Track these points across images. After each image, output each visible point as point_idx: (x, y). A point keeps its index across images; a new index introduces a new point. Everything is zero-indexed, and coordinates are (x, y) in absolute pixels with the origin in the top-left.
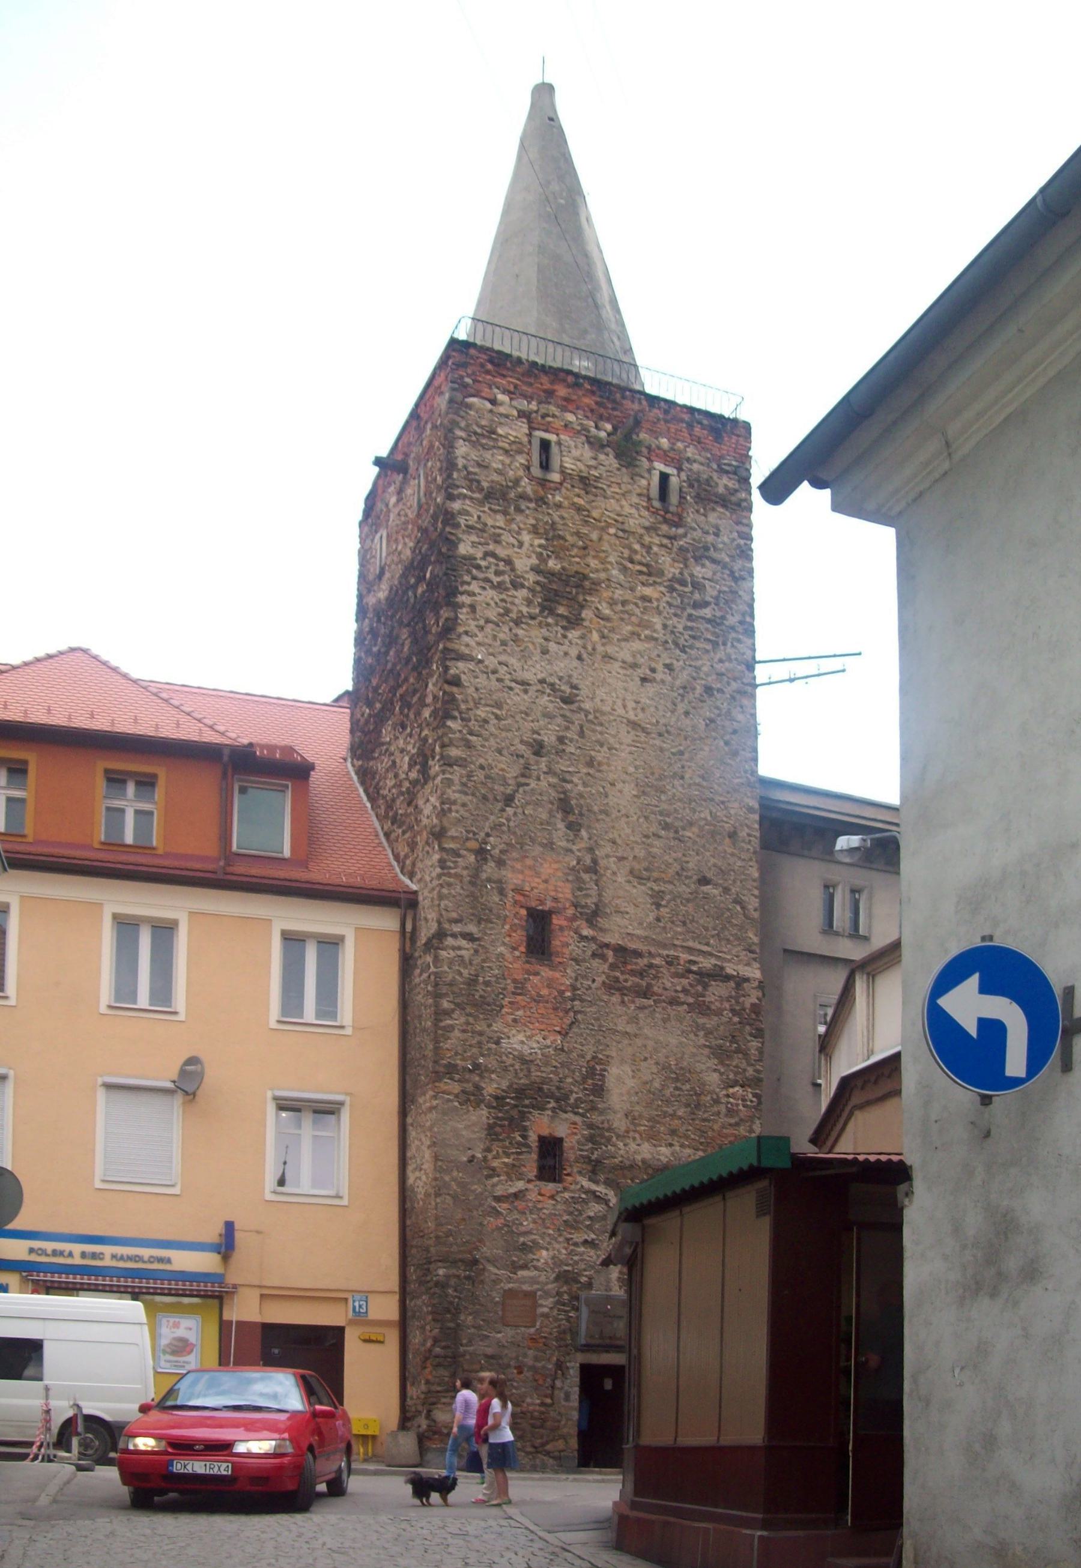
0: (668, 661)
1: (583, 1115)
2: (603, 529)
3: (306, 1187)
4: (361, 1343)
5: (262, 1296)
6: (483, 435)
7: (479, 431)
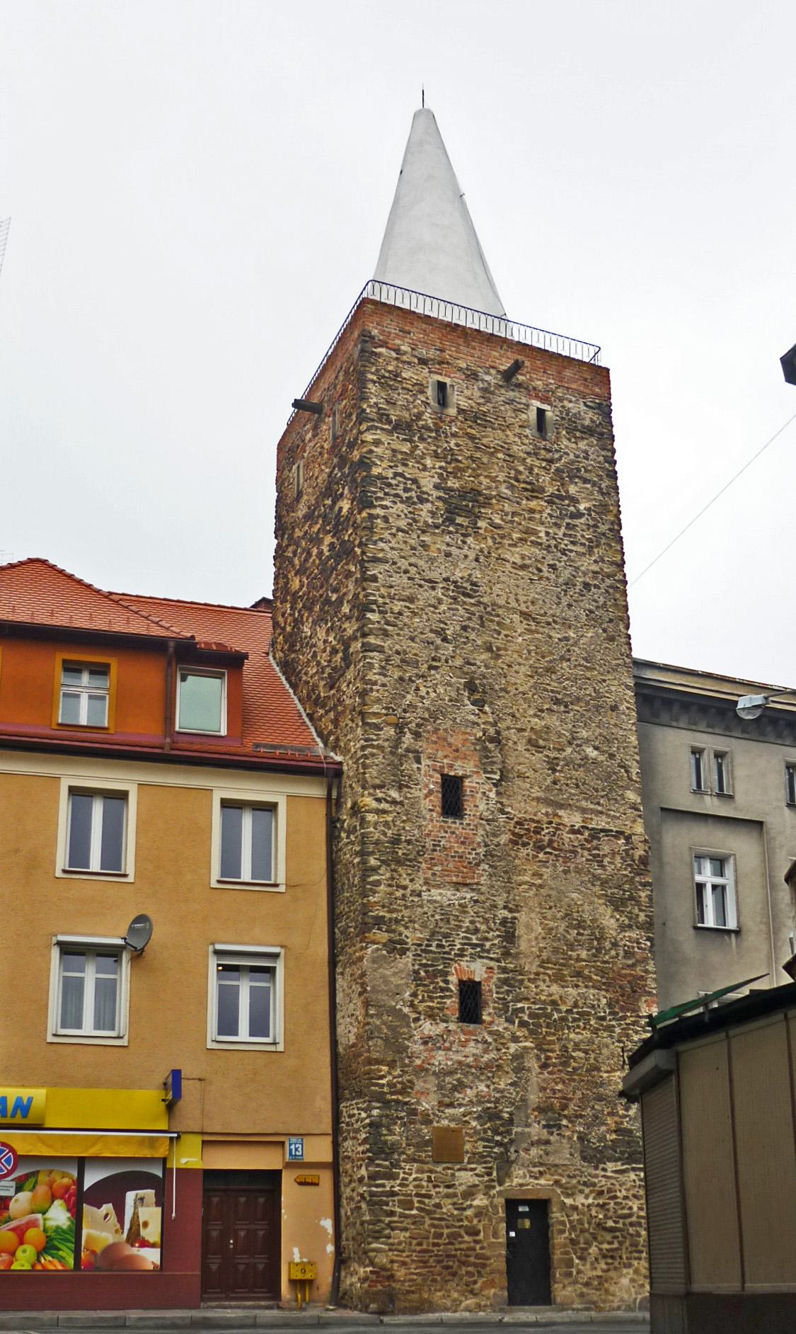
1: (498, 960)
2: (492, 454)
5: (204, 1142)
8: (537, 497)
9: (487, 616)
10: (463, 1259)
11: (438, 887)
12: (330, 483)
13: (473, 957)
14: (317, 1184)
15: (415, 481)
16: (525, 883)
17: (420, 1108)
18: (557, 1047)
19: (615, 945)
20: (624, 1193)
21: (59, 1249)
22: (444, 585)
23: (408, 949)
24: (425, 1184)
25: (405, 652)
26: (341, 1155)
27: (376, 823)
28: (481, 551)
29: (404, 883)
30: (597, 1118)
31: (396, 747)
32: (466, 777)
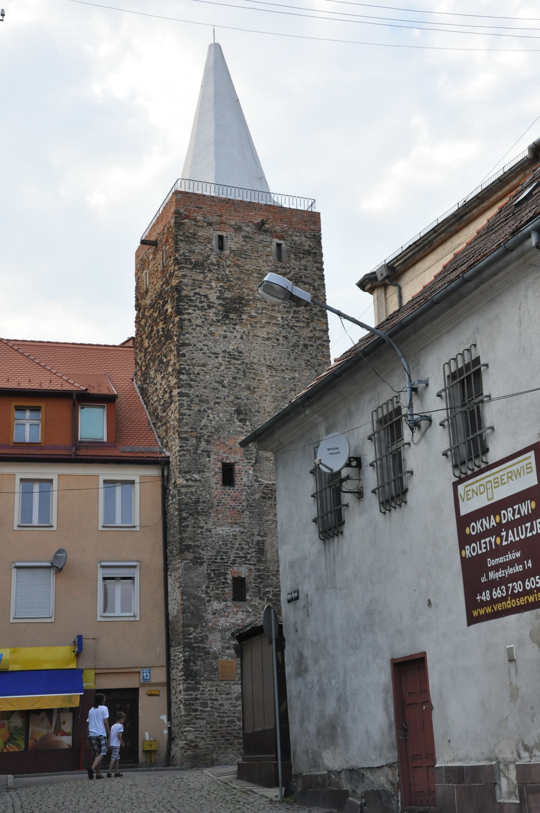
0: (285, 335)
1: (255, 565)
2: (250, 274)
3: (118, 612)
4: (148, 697)
5: (96, 674)
6: (191, 237)
7: (189, 235)
9: (248, 370)
10: (236, 735)
11: (221, 526)
12: (161, 291)
13: (240, 564)
14: (159, 695)
15: (206, 296)
16: (270, 520)
17: (212, 650)
21: (16, 740)
23: (204, 562)
24: (214, 693)
25: (201, 396)
26: (172, 678)
27: (186, 493)
28: (244, 332)
31: (197, 449)
32: (235, 463)
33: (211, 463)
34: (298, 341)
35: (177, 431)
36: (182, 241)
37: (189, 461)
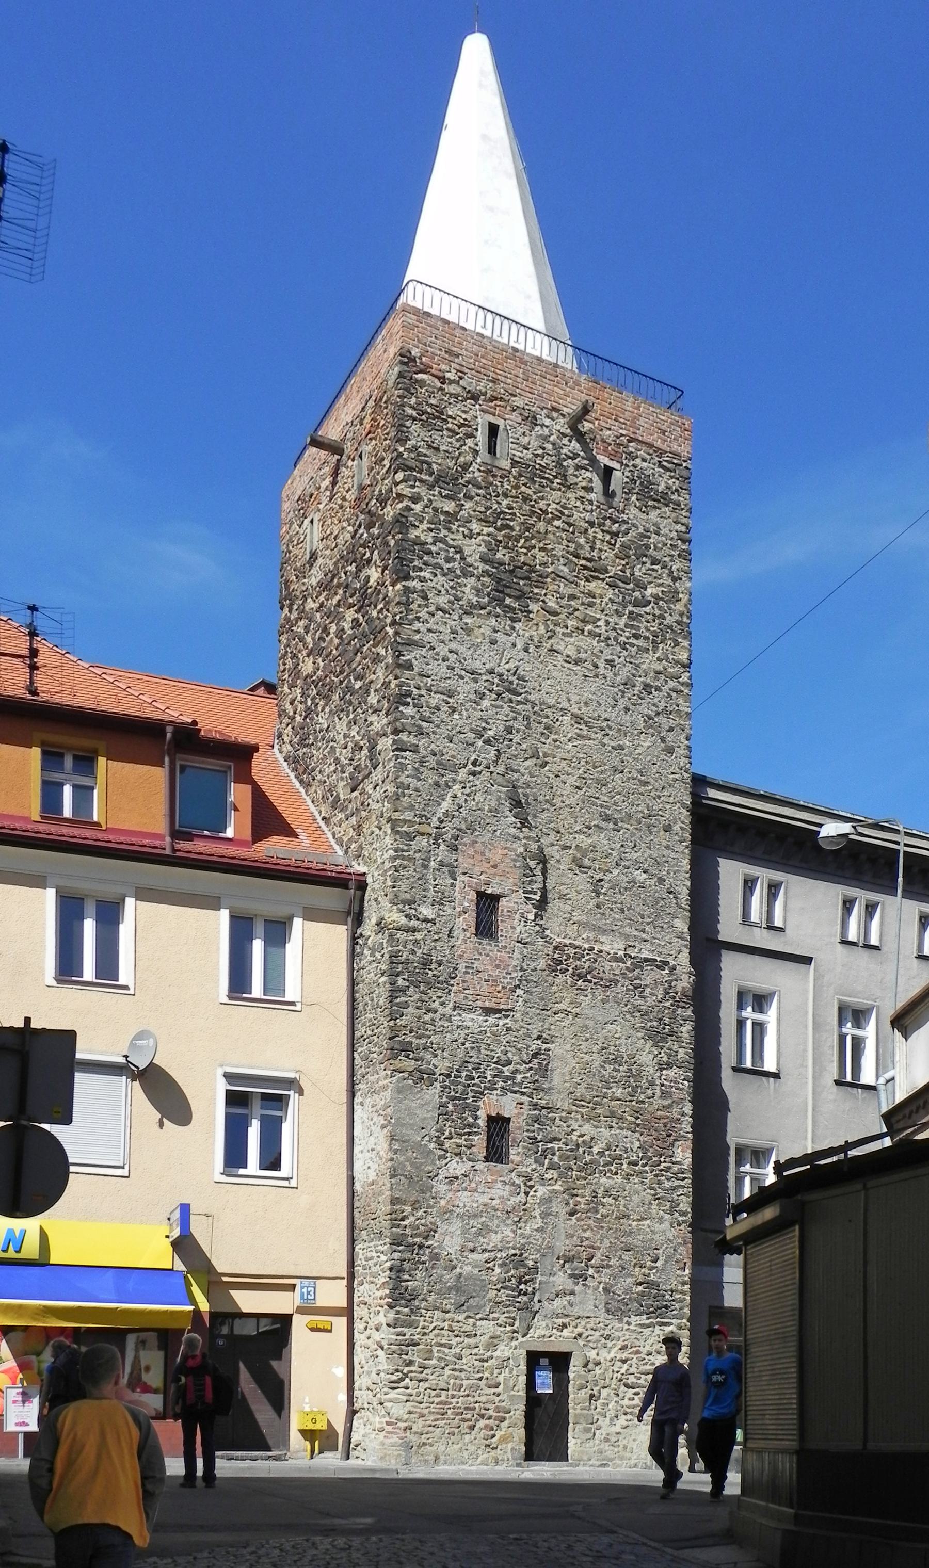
8: (597, 578)
14: (330, 1331)
15: (459, 550)
18: (588, 1192)
19: (652, 1084)
20: (648, 1348)
22: (489, 677)
26: (356, 1300)
28: (531, 638)
29: (434, 1006)
30: (623, 1268)
33: (457, 889)
34: (634, 676)
35: (389, 820)
36: (414, 419)
37: (412, 880)
